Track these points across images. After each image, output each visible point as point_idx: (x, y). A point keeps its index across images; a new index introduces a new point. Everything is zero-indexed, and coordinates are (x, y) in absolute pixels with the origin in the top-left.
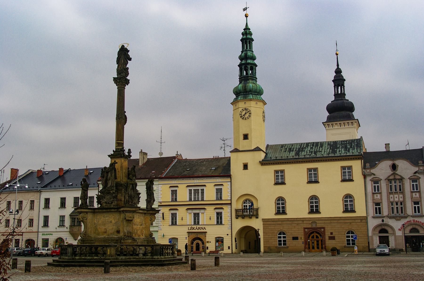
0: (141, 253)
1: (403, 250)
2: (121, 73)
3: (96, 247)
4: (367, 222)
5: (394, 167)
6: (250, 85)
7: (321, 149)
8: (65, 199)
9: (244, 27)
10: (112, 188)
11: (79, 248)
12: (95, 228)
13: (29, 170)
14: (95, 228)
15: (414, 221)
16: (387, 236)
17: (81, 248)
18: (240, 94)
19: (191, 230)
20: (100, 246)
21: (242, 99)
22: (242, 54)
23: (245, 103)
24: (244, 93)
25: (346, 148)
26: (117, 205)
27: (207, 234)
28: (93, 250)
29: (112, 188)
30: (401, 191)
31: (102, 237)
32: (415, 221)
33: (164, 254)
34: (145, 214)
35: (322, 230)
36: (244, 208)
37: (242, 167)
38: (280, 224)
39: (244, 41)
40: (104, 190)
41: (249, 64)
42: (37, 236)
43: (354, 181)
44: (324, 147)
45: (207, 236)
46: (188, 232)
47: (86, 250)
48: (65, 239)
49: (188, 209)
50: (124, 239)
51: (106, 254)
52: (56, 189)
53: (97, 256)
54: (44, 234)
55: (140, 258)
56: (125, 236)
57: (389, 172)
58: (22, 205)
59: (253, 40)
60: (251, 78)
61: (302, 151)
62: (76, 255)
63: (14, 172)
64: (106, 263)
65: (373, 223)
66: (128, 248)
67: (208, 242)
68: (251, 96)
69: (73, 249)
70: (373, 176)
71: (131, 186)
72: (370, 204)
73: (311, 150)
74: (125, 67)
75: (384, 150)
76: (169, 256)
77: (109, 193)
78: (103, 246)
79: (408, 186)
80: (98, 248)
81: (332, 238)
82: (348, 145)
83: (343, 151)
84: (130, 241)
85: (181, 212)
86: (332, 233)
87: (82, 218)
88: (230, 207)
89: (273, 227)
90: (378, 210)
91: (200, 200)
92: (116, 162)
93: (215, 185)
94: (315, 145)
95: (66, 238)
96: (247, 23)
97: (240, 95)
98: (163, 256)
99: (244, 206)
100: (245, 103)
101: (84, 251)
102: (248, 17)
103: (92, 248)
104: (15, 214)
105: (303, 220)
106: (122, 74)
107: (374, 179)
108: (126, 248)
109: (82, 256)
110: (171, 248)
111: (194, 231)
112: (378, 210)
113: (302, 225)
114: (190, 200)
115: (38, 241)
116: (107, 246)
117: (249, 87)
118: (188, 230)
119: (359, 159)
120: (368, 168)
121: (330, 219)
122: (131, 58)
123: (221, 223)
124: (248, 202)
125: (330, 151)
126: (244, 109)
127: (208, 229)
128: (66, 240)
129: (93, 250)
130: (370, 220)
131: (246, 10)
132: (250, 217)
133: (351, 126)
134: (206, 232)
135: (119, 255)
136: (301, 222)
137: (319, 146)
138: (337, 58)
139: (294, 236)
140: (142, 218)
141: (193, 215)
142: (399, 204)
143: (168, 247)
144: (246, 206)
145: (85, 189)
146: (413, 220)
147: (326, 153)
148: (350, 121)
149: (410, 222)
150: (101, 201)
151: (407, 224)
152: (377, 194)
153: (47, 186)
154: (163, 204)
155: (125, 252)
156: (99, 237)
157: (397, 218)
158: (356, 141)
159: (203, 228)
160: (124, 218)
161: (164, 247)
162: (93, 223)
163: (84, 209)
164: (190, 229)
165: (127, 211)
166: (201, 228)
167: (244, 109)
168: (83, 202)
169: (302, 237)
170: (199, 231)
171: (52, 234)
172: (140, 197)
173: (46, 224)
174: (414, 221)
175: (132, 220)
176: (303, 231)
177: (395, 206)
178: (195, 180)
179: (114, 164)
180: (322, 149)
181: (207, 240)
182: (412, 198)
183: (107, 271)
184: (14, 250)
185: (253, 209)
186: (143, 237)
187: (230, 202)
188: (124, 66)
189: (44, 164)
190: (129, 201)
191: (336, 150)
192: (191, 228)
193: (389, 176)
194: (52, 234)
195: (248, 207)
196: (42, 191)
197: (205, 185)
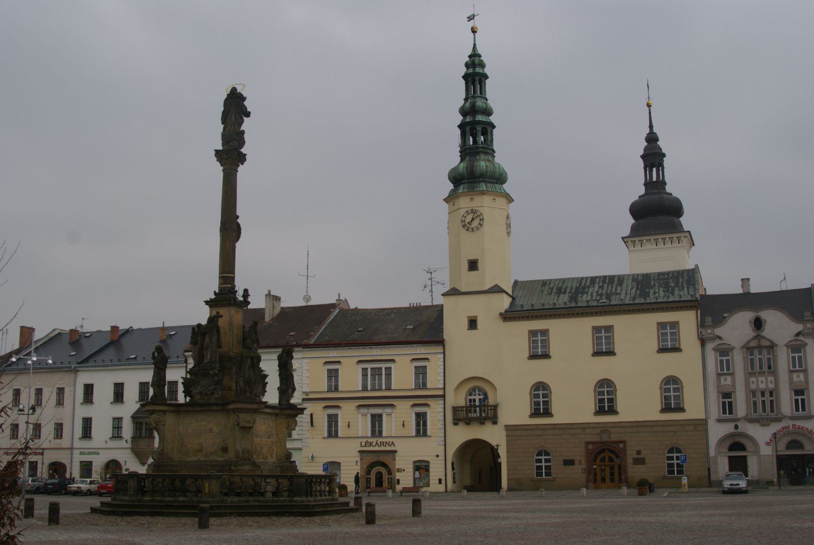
1: (773, 482)
3: (183, 479)
5: (758, 324)
7: (619, 288)
9: (470, 52)
11: (150, 480)
17: (153, 480)
18: (463, 182)
19: (365, 446)
20: (191, 476)
21: (465, 191)
22: (465, 103)
23: (471, 199)
24: (470, 180)
27: (397, 454)
28: (177, 483)
31: (194, 459)
33: (314, 494)
34: (276, 415)
35: (621, 445)
36: (470, 405)
37: (479, 324)
39: (470, 79)
41: (480, 122)
42: (70, 456)
44: (624, 286)
45: (397, 458)
46: (360, 452)
48: (124, 463)
49: (360, 406)
51: (202, 492)
52: (106, 366)
53: (185, 496)
54: (83, 452)
56: (238, 458)
57: (749, 332)
58: (42, 397)
60: (484, 150)
61: (583, 293)
62: (144, 493)
65: (717, 432)
67: (399, 470)
68: (484, 185)
70: (718, 342)
73: (600, 292)
81: (639, 461)
82: (671, 281)
83: (662, 294)
84: (248, 468)
85: (347, 413)
86: (639, 452)
87: (156, 423)
88: (443, 402)
90: (728, 407)
91: (384, 388)
93: (413, 360)
94: (607, 281)
95: (126, 461)
96: (475, 45)
97: (461, 184)
98: (312, 496)
99: (470, 400)
100: (472, 200)
102: (476, 32)
103: (175, 480)
104: (28, 414)
109: (155, 495)
114: (365, 388)
115: (71, 466)
117: (478, 168)
119: (691, 308)
120: (709, 326)
123: (425, 434)
124: (477, 392)
126: (470, 212)
128: (125, 464)
129: (177, 483)
132: (482, 421)
134: (395, 452)
135: (226, 494)
138: (650, 113)
142: (767, 394)
143: (321, 480)
144: (474, 400)
146: (793, 425)
147: (628, 296)
148: (674, 235)
150: (192, 390)
152: (727, 377)
154: (311, 396)
156: (188, 460)
157: (764, 422)
158: (685, 274)
159: (390, 443)
160: (236, 423)
161: (314, 480)
162: (176, 433)
163: (159, 405)
164: (363, 444)
165: (241, 410)
166: (386, 442)
168: (156, 392)
169: (581, 461)
170: (382, 448)
171: (98, 454)
172: (267, 383)
173: (87, 433)
179: (216, 319)
180: (621, 290)
181: (397, 466)
183: (203, 525)
184: (28, 481)
188: (236, 127)
191: (649, 292)
192: (366, 442)
194: (98, 454)
195: (477, 403)
196: (79, 371)
197: (339, 362)
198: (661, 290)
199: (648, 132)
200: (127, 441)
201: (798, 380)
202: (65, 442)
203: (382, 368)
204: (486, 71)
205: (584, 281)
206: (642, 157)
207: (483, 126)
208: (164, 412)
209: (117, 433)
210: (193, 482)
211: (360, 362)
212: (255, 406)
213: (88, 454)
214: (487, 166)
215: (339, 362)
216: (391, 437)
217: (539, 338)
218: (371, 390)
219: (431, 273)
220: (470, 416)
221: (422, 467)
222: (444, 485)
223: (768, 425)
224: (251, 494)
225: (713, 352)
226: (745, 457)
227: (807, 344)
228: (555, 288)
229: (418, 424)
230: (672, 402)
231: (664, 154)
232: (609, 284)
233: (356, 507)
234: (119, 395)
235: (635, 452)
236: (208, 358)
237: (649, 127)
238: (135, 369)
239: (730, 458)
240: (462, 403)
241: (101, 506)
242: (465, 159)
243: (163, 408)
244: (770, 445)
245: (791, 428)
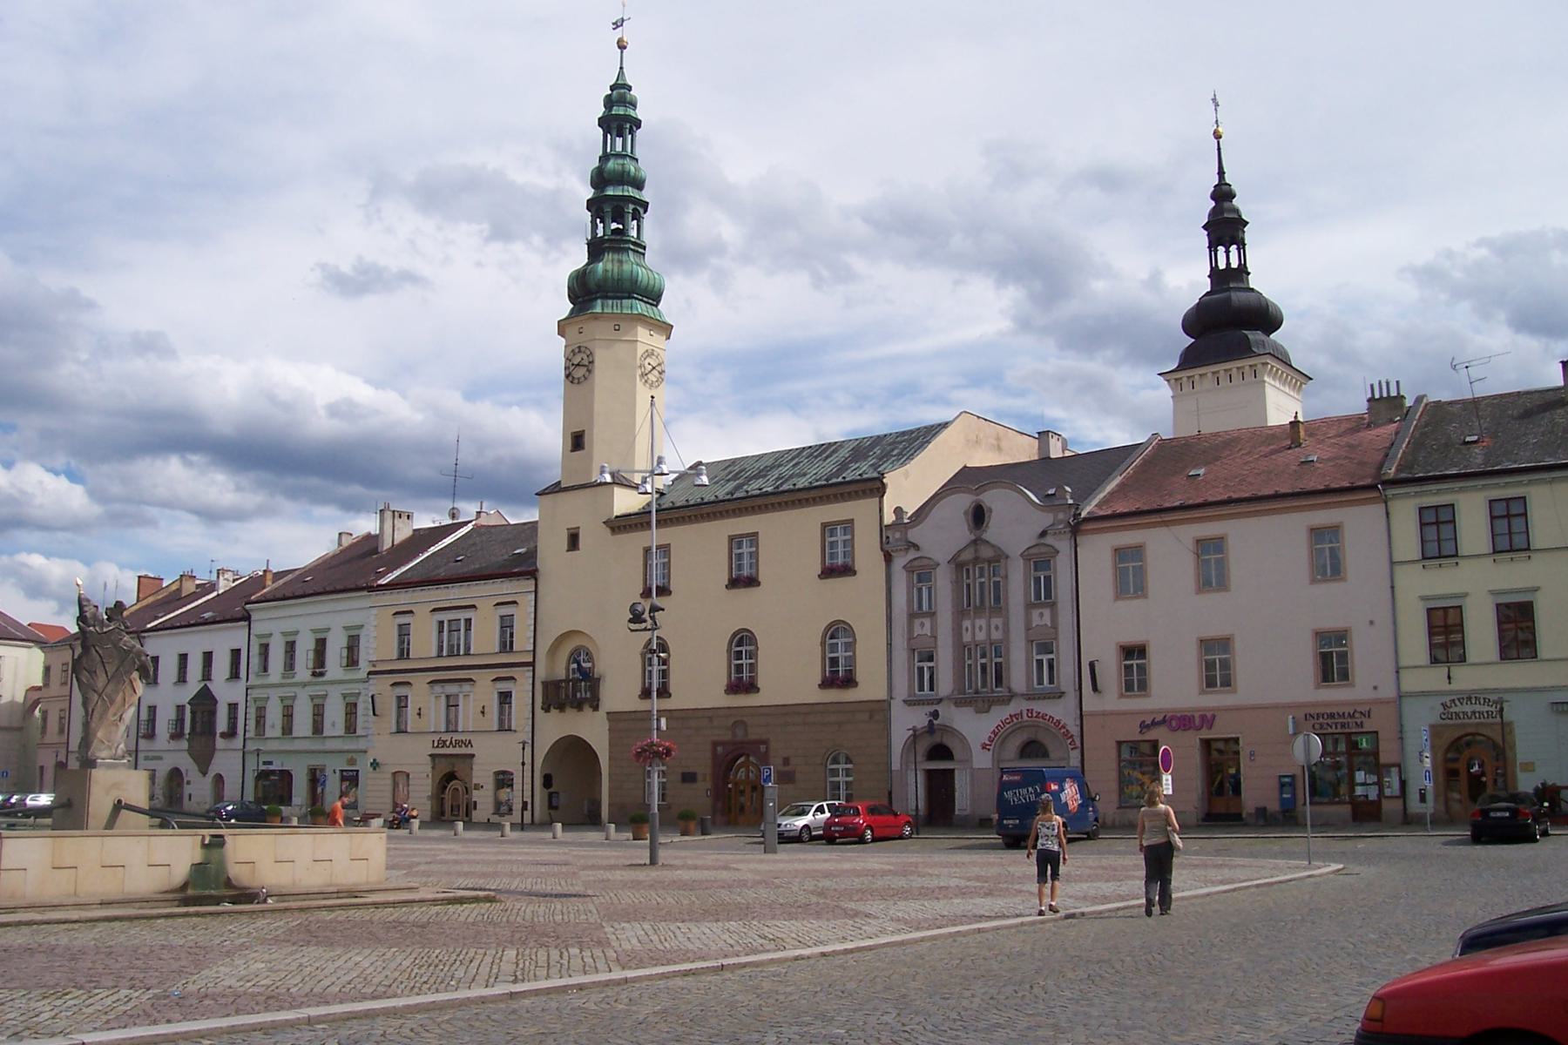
1: (991, 820)
15: (1032, 713)
16: (949, 770)
19: (437, 747)
30: (997, 604)
32: (1035, 715)
35: (719, 749)
43: (858, 573)
46: (430, 755)
65: (905, 722)
70: (912, 554)
72: (901, 657)
85: (420, 693)
86: (786, 761)
90: (925, 678)
93: (434, 610)
102: (625, 48)
105: (710, 714)
107: (916, 563)
114: (440, 655)
118: (433, 747)
126: (577, 351)
130: (897, 709)
131: (622, 25)
134: (473, 756)
138: (1219, 149)
146: (1028, 710)
149: (1017, 719)
151: (1008, 726)
152: (923, 620)
157: (982, 703)
174: (1030, 715)
176: (709, 755)
181: (475, 781)
182: (1028, 628)
187: (531, 660)
189: (212, 561)
193: (960, 552)
199: (1217, 183)
201: (1041, 624)
203: (460, 620)
204: (639, 113)
207: (615, 203)
218: (449, 656)
221: (503, 780)
223: (987, 711)
230: (840, 669)
231: (588, 209)
237: (1219, 173)
238: (199, 631)
240: (561, 674)
244: (989, 750)
245: (1025, 717)
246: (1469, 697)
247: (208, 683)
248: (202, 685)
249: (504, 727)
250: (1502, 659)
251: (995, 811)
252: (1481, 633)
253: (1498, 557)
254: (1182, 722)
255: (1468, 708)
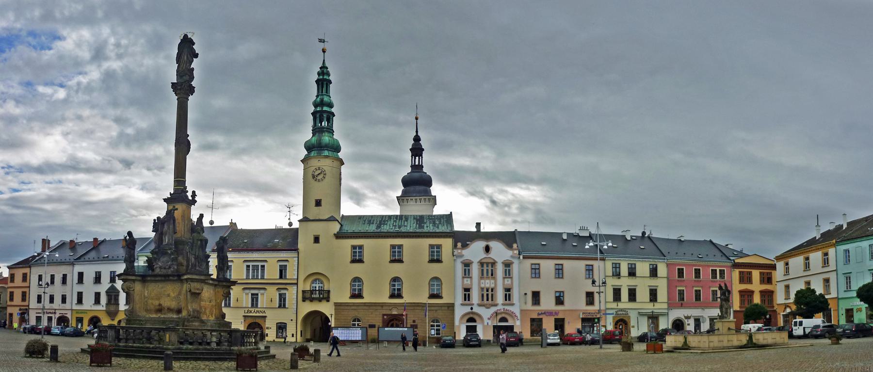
0: (214, 342)
2: (183, 76)
4: (453, 310)
5: (487, 249)
6: (326, 139)
7: (406, 222)
8: (100, 273)
10: (171, 246)
11: (125, 330)
12: (146, 303)
13: (61, 241)
14: (146, 303)
17: (127, 330)
20: (156, 329)
21: (315, 155)
22: (316, 99)
25: (434, 223)
26: (177, 270)
27: (267, 318)
29: (171, 246)
33: (245, 344)
34: (216, 285)
37: (321, 240)
38: (355, 310)
39: (320, 83)
40: (157, 250)
41: (326, 112)
44: (409, 221)
45: (266, 321)
46: (244, 316)
47: (134, 334)
49: (244, 289)
50: (188, 321)
52: (90, 261)
55: (213, 349)
56: (190, 316)
57: (482, 255)
59: (330, 82)
60: (328, 130)
61: (384, 224)
62: (119, 340)
63: (45, 243)
64: (167, 355)
66: (195, 334)
67: (267, 328)
68: (327, 152)
69: (115, 332)
71: (199, 242)
73: (394, 224)
74: (189, 68)
75: (474, 230)
76: (252, 347)
77: (164, 253)
78: (159, 330)
79: (500, 270)
80: (151, 331)
82: (436, 220)
83: (432, 228)
84: (197, 324)
86: (414, 321)
87: (128, 289)
88: (296, 287)
89: (347, 313)
91: (260, 278)
92: (176, 207)
93: (279, 261)
94: (398, 218)
96: (324, 60)
97: (313, 151)
98: (244, 346)
101: (132, 335)
102: (325, 52)
104: (45, 288)
105: (382, 305)
106: (184, 77)
108: (192, 333)
110: (254, 336)
111: (251, 314)
112: (467, 297)
113: (380, 311)
114: (248, 278)
116: (164, 330)
119: (450, 237)
120: (459, 249)
121: (414, 305)
122: (198, 54)
123: (284, 307)
125: (416, 226)
126: (317, 169)
127: (268, 313)
132: (320, 300)
133: (428, 203)
135: (181, 343)
136: (380, 308)
137: (404, 219)
138: (417, 123)
139: (371, 324)
140: (212, 292)
141: (250, 295)
142: (490, 290)
143: (250, 334)
145: (131, 247)
147: (412, 228)
148: (427, 198)
153: (80, 259)
155: (190, 339)
157: (488, 307)
158: (444, 217)
160: (188, 290)
161: (246, 334)
165: (192, 280)
167: (317, 169)
170: (258, 314)
172: (209, 261)
173: (80, 301)
175: (200, 293)
176: (381, 318)
177: (485, 293)
178: (254, 254)
179: (172, 211)
180: (408, 224)
181: (267, 326)
182: (504, 284)
185: (324, 291)
186: (213, 319)
187: (296, 282)
188: (188, 65)
190: (195, 265)
191: (424, 226)
195: (317, 289)
196: (75, 264)
198: (431, 225)
200: (103, 306)
202: (67, 306)
204: (331, 78)
205: (384, 217)
206: (411, 150)
208: (134, 281)
209: (97, 301)
210: (157, 333)
211: (245, 261)
212: (202, 277)
213: (81, 313)
214: (329, 140)
215: (287, 261)
216: (263, 308)
217: (357, 250)
219: (290, 208)
220: (313, 296)
222: (295, 338)
224: (200, 344)
225: (461, 264)
226: (476, 326)
227: (513, 263)
228: (367, 221)
229: (252, 300)
232: (399, 219)
233: (266, 350)
234: (98, 279)
235: (412, 321)
236: (166, 240)
239: (467, 327)
241: (88, 348)
242: (316, 134)
243: (133, 278)
246: (622, 310)
247: (114, 284)
248: (111, 285)
249: (282, 305)
250: (629, 301)
251: (120, 312)
252: (625, 295)
253: (614, 277)
254: (549, 313)
255: (621, 313)
